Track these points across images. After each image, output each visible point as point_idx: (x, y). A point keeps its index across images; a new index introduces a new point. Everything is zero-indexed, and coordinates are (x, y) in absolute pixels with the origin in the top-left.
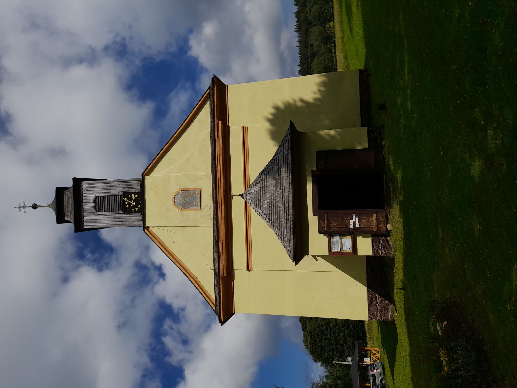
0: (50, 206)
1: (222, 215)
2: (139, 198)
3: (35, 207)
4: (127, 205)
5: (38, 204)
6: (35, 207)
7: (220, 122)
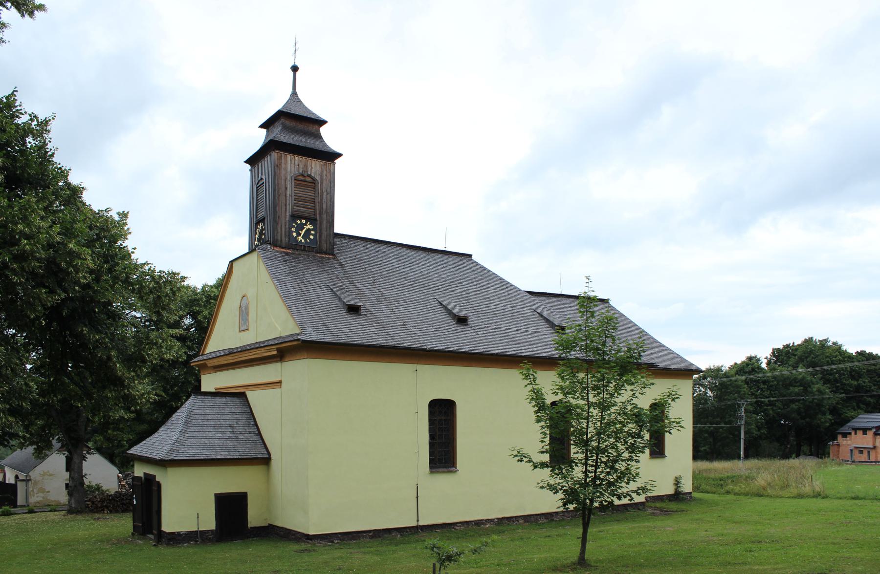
0: (294, 93)
1: (230, 359)
2: (308, 241)
3: (295, 69)
4: (301, 221)
5: (297, 73)
6: (295, 69)
7: (275, 353)
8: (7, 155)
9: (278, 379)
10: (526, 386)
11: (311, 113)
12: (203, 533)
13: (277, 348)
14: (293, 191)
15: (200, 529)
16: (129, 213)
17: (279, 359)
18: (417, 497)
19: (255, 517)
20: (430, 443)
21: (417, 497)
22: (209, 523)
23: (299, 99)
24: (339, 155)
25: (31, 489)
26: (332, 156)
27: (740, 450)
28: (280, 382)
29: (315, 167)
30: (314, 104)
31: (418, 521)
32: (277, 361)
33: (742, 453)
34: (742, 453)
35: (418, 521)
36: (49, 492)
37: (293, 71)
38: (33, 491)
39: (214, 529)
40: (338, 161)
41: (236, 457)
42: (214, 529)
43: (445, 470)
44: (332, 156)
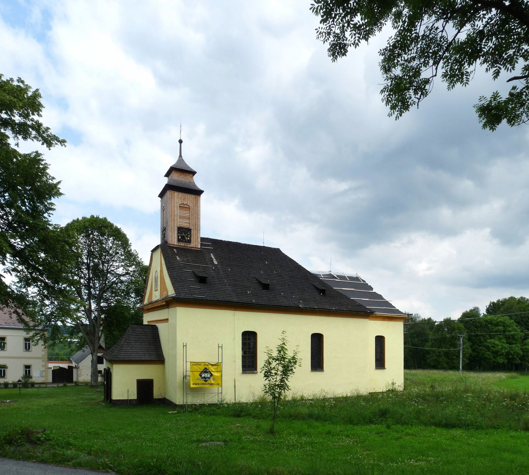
3: (181, 142)
5: (182, 144)
6: (181, 142)
7: (164, 303)
8: (6, 168)
9: (166, 318)
10: (462, 86)
11: (189, 167)
12: (131, 400)
13: (165, 301)
14: (178, 213)
15: (130, 398)
16: (62, 196)
17: (167, 307)
18: (235, 386)
19: (157, 394)
20: (242, 356)
21: (235, 386)
22: (134, 396)
23: (183, 159)
24: (202, 192)
25: (79, 373)
26: (198, 192)
27: (460, 364)
28: (167, 319)
29: (189, 199)
30: (191, 163)
31: (235, 400)
32: (166, 308)
33: (461, 367)
34: (461, 367)
35: (235, 400)
36: (294, 373)
37: (180, 143)
38: (80, 374)
39: (136, 399)
40: (202, 196)
41: (136, 359)
42: (136, 399)
43: (251, 372)
44: (198, 192)
